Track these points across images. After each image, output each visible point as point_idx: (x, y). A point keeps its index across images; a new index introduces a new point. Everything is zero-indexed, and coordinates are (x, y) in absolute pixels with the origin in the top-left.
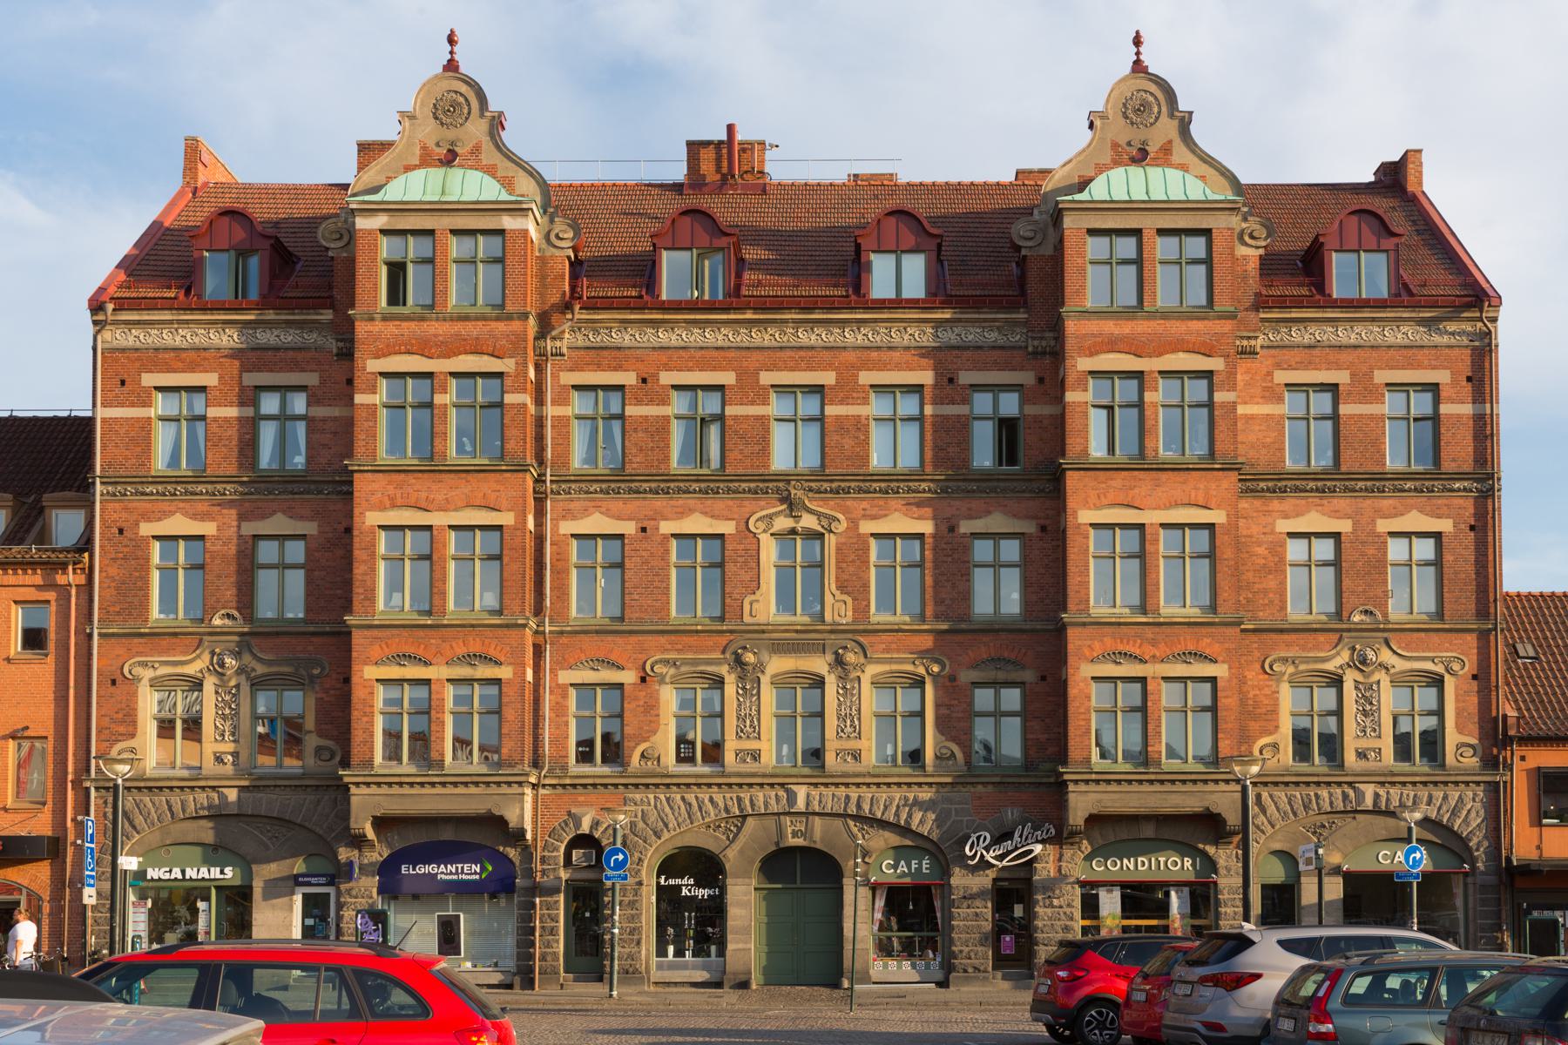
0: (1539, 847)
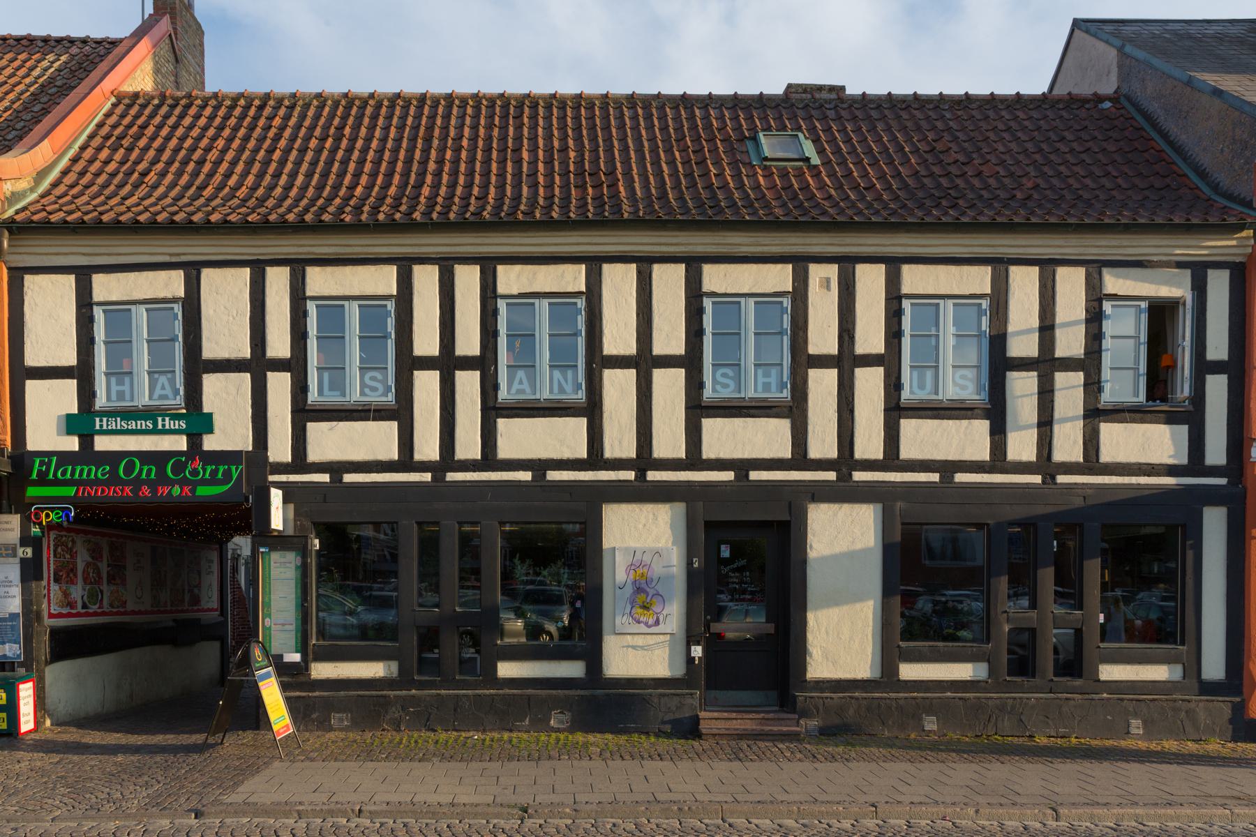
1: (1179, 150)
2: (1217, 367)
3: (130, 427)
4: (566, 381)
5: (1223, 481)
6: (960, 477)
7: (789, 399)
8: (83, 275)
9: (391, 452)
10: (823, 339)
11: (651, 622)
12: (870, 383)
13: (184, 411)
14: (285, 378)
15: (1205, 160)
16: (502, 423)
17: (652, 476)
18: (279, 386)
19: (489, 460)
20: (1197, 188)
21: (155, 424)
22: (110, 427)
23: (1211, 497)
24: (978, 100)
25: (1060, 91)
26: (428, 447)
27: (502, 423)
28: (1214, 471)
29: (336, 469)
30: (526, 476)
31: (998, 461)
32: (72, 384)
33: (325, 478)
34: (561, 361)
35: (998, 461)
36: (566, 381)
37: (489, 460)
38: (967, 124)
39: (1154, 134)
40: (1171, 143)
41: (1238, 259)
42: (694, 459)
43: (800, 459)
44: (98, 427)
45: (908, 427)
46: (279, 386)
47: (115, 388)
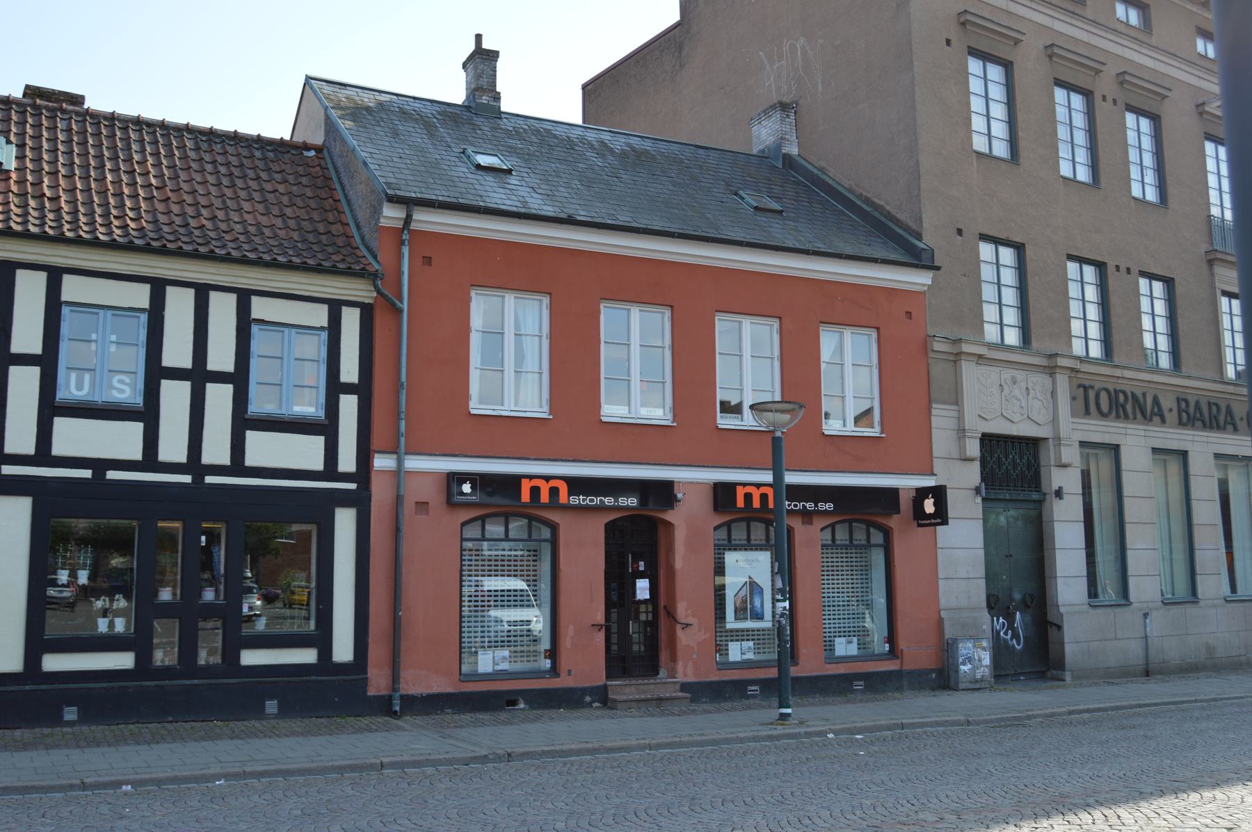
2: (349, 389)
5: (353, 486)
6: (112, 475)
7: (141, 405)
10: (177, 352)
12: (219, 398)
16: (250, 435)
23: (344, 499)
24: (247, 139)
25: (299, 139)
27: (250, 435)
28: (346, 477)
31: (150, 460)
35: (150, 460)
38: (245, 161)
39: (338, 186)
41: (367, 301)
45: (252, 437)
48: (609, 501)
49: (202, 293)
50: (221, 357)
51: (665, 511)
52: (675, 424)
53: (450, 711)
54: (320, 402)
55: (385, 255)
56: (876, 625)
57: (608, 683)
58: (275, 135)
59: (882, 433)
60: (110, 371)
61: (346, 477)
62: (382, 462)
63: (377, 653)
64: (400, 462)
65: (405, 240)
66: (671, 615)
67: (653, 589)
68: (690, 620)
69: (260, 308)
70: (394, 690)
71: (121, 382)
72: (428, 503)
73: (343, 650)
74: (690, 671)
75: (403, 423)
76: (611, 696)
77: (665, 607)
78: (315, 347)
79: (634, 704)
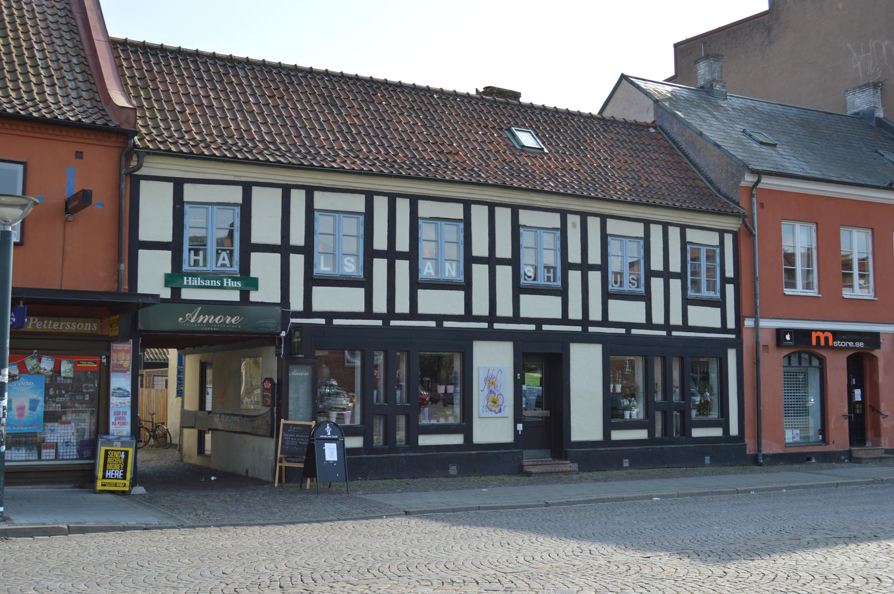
0: (61, 285)
1: (696, 166)
3: (206, 284)
4: (449, 269)
5: (733, 336)
8: (179, 184)
9: (361, 308)
10: (480, 248)
11: (497, 410)
12: (504, 273)
13: (239, 276)
14: (301, 258)
15: (712, 176)
17: (497, 326)
18: (297, 262)
19: (413, 314)
20: (709, 188)
21: (222, 283)
22: (193, 284)
26: (380, 305)
28: (658, 327)
29: (329, 316)
30: (432, 324)
32: (169, 254)
33: (322, 321)
34: (711, 287)
36: (449, 269)
37: (413, 314)
40: (691, 161)
42: (516, 318)
43: (468, 315)
44: (185, 283)
46: (297, 262)
47: (193, 257)
48: (851, 344)
49: (392, 198)
50: (504, 250)
51: (873, 350)
52: (876, 299)
53: (782, 463)
54: (461, 270)
55: (743, 203)
56: (813, 422)
57: (852, 448)
58: (585, 110)
59: (875, 296)
60: (344, 254)
61: (658, 327)
62: (749, 323)
63: (748, 431)
64: (756, 322)
65: (754, 195)
66: (876, 411)
67: (863, 396)
68: (887, 413)
69: (525, 217)
70: (759, 450)
71: (349, 261)
72: (767, 346)
73: (734, 431)
74: (887, 442)
75: (758, 300)
76: (854, 455)
77: (870, 405)
78: (354, 226)
79: (869, 461)
